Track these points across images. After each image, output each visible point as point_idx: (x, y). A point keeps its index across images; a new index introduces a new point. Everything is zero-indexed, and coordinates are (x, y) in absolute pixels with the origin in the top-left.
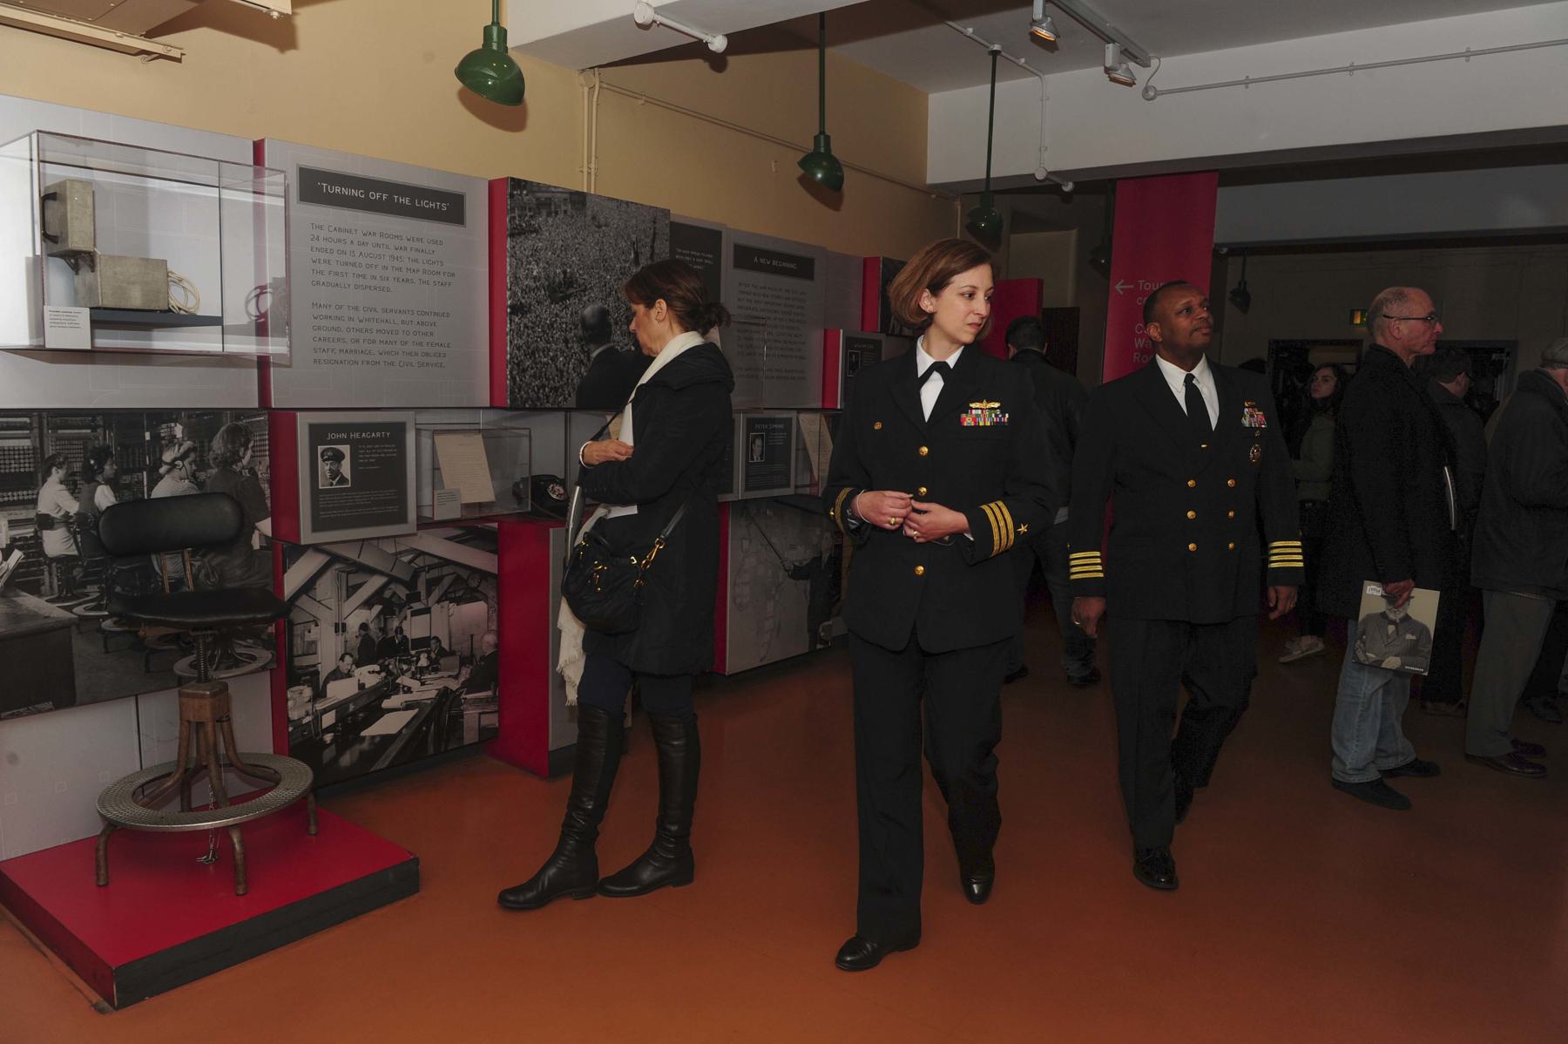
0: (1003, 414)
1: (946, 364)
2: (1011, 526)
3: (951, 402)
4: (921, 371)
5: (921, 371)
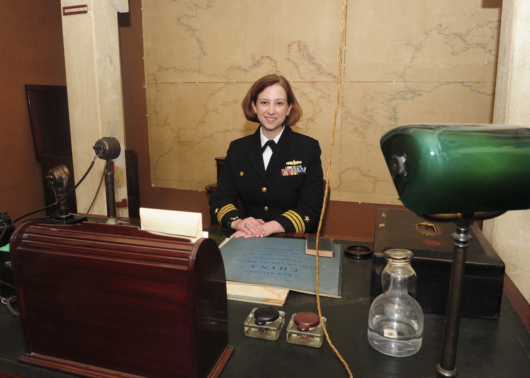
0: (303, 167)
1: (273, 142)
2: (302, 221)
3: (278, 161)
4: (263, 145)
5: (263, 145)
